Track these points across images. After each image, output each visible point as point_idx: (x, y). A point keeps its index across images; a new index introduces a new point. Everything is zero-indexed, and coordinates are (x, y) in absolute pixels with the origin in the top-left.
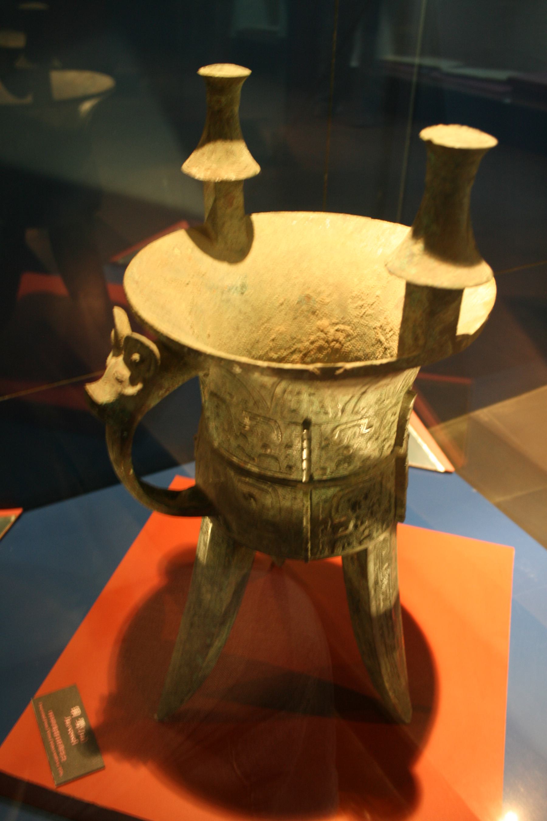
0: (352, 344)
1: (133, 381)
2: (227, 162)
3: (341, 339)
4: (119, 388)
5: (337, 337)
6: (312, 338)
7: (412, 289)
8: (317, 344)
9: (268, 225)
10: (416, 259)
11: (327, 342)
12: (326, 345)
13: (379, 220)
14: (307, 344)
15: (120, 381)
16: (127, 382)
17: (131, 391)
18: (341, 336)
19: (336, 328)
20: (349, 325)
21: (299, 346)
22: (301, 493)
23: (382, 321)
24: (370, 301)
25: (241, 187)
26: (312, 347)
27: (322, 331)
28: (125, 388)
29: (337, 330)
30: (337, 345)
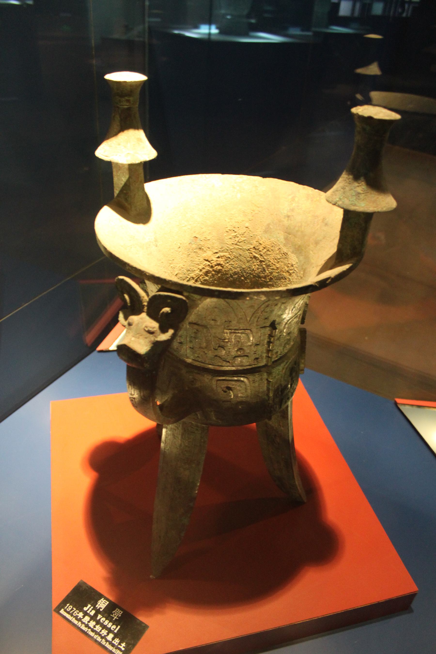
0: (230, 265)
1: (163, 330)
2: (127, 148)
3: (222, 263)
4: (152, 338)
5: (218, 262)
6: (200, 267)
7: (347, 214)
8: (204, 271)
9: (156, 190)
10: (362, 196)
11: (212, 267)
12: (211, 269)
13: (276, 179)
14: (197, 272)
15: (151, 333)
16: (159, 331)
17: (164, 337)
18: (221, 261)
19: (218, 255)
20: (226, 252)
21: (192, 275)
22: (265, 374)
23: (255, 243)
24: (241, 232)
25: (142, 165)
26: (201, 273)
27: (207, 260)
28: (156, 337)
29: (218, 257)
30: (219, 268)
